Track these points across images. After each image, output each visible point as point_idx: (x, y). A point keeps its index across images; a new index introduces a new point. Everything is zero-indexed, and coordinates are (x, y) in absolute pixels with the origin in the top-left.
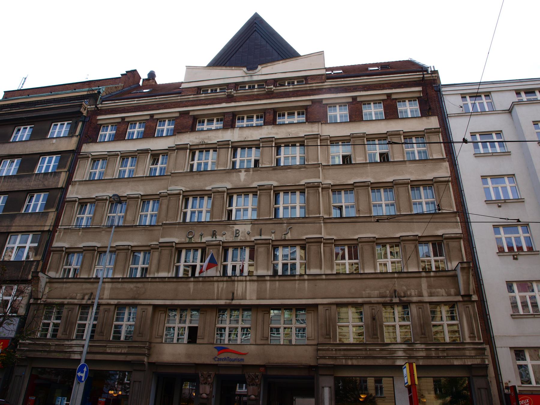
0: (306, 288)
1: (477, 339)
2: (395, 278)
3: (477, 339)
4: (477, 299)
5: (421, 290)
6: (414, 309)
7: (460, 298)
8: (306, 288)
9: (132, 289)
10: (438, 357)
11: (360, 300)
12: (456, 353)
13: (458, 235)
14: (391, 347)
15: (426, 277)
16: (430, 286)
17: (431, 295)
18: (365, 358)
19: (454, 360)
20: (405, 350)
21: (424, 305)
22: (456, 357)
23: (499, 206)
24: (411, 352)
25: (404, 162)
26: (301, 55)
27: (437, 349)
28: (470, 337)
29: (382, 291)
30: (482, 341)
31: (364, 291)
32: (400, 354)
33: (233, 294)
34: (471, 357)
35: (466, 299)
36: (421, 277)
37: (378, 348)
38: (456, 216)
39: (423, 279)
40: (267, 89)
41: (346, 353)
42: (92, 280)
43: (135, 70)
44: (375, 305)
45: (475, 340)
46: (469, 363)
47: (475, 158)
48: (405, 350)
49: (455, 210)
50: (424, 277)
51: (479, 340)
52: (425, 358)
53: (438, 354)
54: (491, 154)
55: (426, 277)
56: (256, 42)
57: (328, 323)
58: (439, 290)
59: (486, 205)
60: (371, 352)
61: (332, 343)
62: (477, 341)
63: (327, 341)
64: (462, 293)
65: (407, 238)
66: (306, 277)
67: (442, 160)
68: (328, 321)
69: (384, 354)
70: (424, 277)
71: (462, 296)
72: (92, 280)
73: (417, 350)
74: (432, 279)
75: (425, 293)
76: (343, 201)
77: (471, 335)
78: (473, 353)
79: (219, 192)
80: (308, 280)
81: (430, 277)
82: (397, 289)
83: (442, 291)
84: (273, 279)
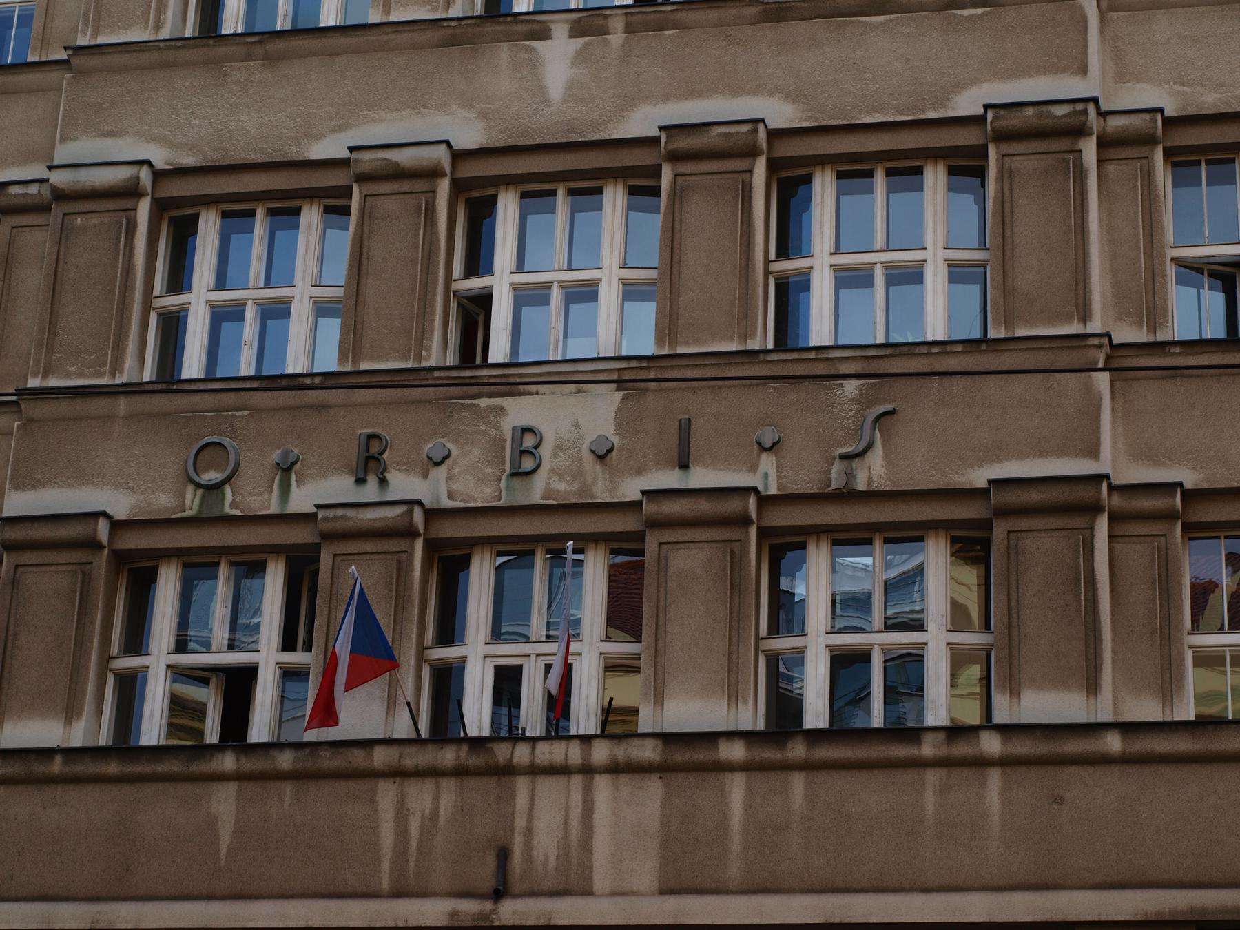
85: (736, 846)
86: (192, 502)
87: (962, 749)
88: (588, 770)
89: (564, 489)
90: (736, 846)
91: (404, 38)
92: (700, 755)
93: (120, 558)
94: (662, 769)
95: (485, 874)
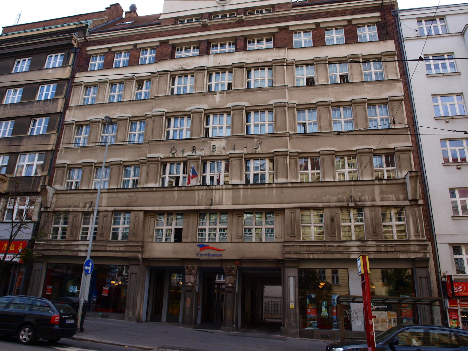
1: (421, 237)
2: (351, 185)
3: (421, 237)
5: (374, 195)
6: (367, 212)
7: (408, 203)
8: (275, 195)
9: (125, 198)
10: (387, 252)
11: (321, 205)
12: (403, 248)
13: (408, 148)
14: (346, 243)
15: (379, 184)
16: (382, 193)
17: (382, 200)
18: (325, 253)
20: (358, 246)
21: (377, 208)
22: (402, 252)
23: (447, 122)
25: (362, 82)
27: (386, 245)
28: (415, 235)
29: (340, 196)
30: (425, 239)
33: (212, 200)
35: (413, 203)
36: (374, 185)
37: (335, 244)
39: (376, 186)
40: (238, 17)
41: (308, 248)
44: (334, 209)
46: (413, 257)
48: (358, 246)
50: (377, 184)
55: (379, 184)
57: (293, 224)
58: (390, 195)
60: (330, 248)
62: (421, 238)
63: (292, 239)
64: (410, 198)
67: (397, 80)
68: (293, 222)
69: (341, 249)
70: (377, 184)
71: (410, 201)
73: (369, 246)
74: (384, 186)
77: (416, 234)
78: (417, 249)
79: (197, 112)
81: (383, 184)
82: (353, 195)
83: (392, 197)
85: (241, 199)
86: (171, 155)
87: (270, 186)
88: (222, 189)
89: (219, 153)
90: (241, 199)
91: (198, 95)
92: (237, 187)
93: (162, 163)
94: (232, 189)
95: (210, 203)
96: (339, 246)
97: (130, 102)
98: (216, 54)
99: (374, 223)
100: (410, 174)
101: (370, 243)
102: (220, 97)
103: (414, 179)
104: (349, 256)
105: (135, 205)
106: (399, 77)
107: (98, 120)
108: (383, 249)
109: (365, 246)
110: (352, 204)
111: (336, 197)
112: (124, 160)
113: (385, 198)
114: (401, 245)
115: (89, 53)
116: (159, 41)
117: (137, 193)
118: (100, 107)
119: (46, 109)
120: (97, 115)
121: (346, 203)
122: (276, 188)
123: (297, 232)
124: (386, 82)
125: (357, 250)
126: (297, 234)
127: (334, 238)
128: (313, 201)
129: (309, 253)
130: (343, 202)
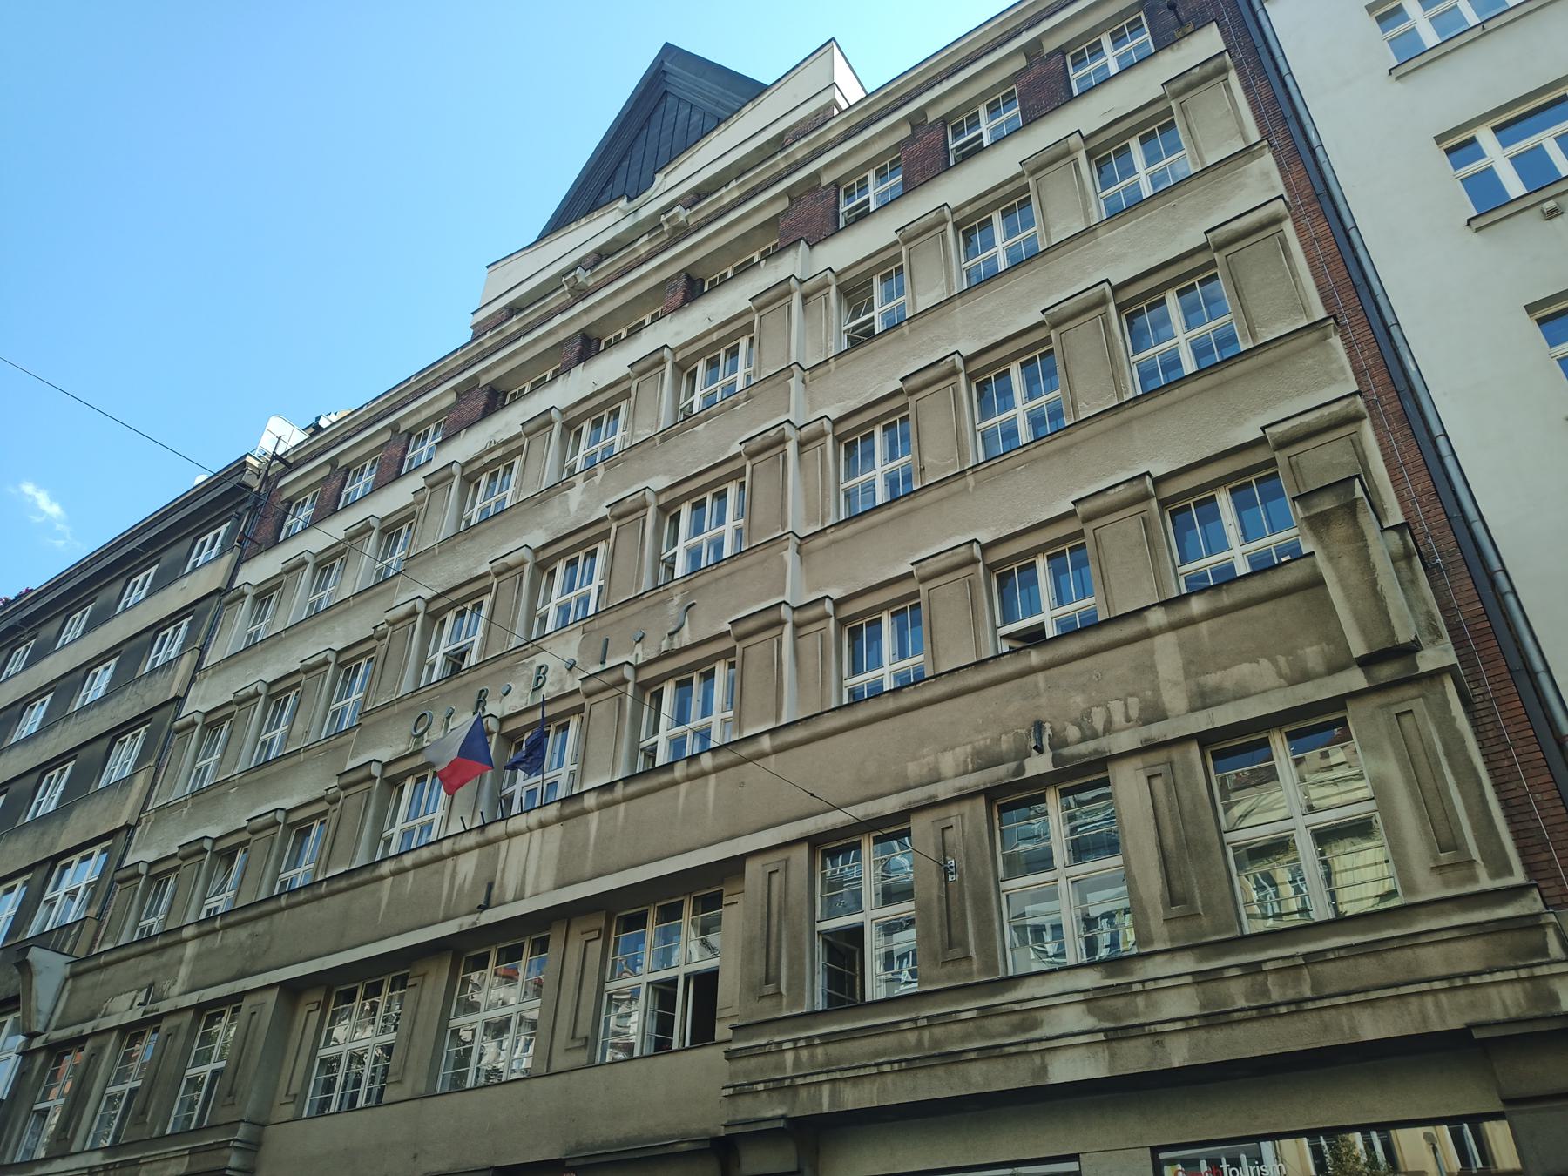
0: (711, 805)
1: (1482, 871)
2: (1032, 671)
3: (1482, 871)
4: (1451, 658)
5: (1156, 690)
6: (1129, 783)
7: (1356, 680)
8: (711, 805)
9: (241, 945)
10: (1265, 1012)
11: (890, 805)
12: (1369, 969)
13: (1335, 408)
14: (1023, 991)
15: (1173, 627)
16: (1194, 664)
17: (1203, 700)
18: (910, 1066)
19: (1355, 1011)
20: (1092, 999)
21: (1175, 754)
22: (1366, 997)
23: (1552, 214)
24: (1119, 1003)
25: (1089, 230)
26: (769, 83)
27: (1253, 969)
28: (1438, 869)
29: (982, 741)
30: (1519, 877)
31: (915, 759)
32: (1073, 1019)
33: (490, 886)
34: (1457, 982)
35: (1386, 672)
36: (1148, 635)
37: (968, 1007)
38: (1327, 337)
39: (1159, 640)
40: (668, 221)
41: (835, 1050)
42: (157, 943)
43: (667, 44)
44: (954, 810)
45: (1474, 879)
46: (1455, 1023)
47: (1398, 84)
48: (1092, 999)
49: (1320, 313)
50: (1161, 631)
51: (1494, 875)
52: (1189, 1024)
53: (1265, 992)
54: (1478, 31)
55: (1173, 627)
56: (675, 100)
57: (774, 930)
58: (1245, 668)
59: (1476, 238)
60: (938, 1032)
61: (786, 1014)
62: (1485, 883)
63: (767, 1010)
64: (1358, 648)
65: (1099, 503)
66: (707, 761)
67: (1248, 152)
68: (774, 921)
69: (998, 1032)
70: (1161, 631)
71: (1365, 663)
72: (157, 943)
73: (1150, 989)
74: (1204, 627)
75: (1175, 700)
76: (1232, 531)
77: (1445, 858)
78: (1468, 955)
79: (509, 568)
80: (717, 769)
81: (1191, 621)
82: (1044, 715)
83: (1259, 672)
84: (607, 797)
96: (985, 1013)
97: (346, 605)
98: (1397, 572)
99: (1170, 839)
100: (1305, 508)
101: (1153, 968)
102: (585, 490)
103: (1340, 530)
104: (1044, 1069)
105: (259, 967)
106: (1255, 136)
107: (252, 690)
108: (1238, 994)
109: (1124, 991)
110: (1039, 765)
111: (969, 748)
112: (288, 804)
113: (1218, 690)
114: (1354, 952)
115: (287, 494)
116: (454, 389)
117: (277, 917)
118: (273, 645)
119: (147, 698)
120: (1410, 925)
121: (1012, 765)
122: (717, 769)
123: (790, 967)
124: (1194, 183)
125: (1090, 1022)
126: (790, 978)
127: (964, 966)
128: (863, 793)
129: (841, 1074)
130: (998, 761)
